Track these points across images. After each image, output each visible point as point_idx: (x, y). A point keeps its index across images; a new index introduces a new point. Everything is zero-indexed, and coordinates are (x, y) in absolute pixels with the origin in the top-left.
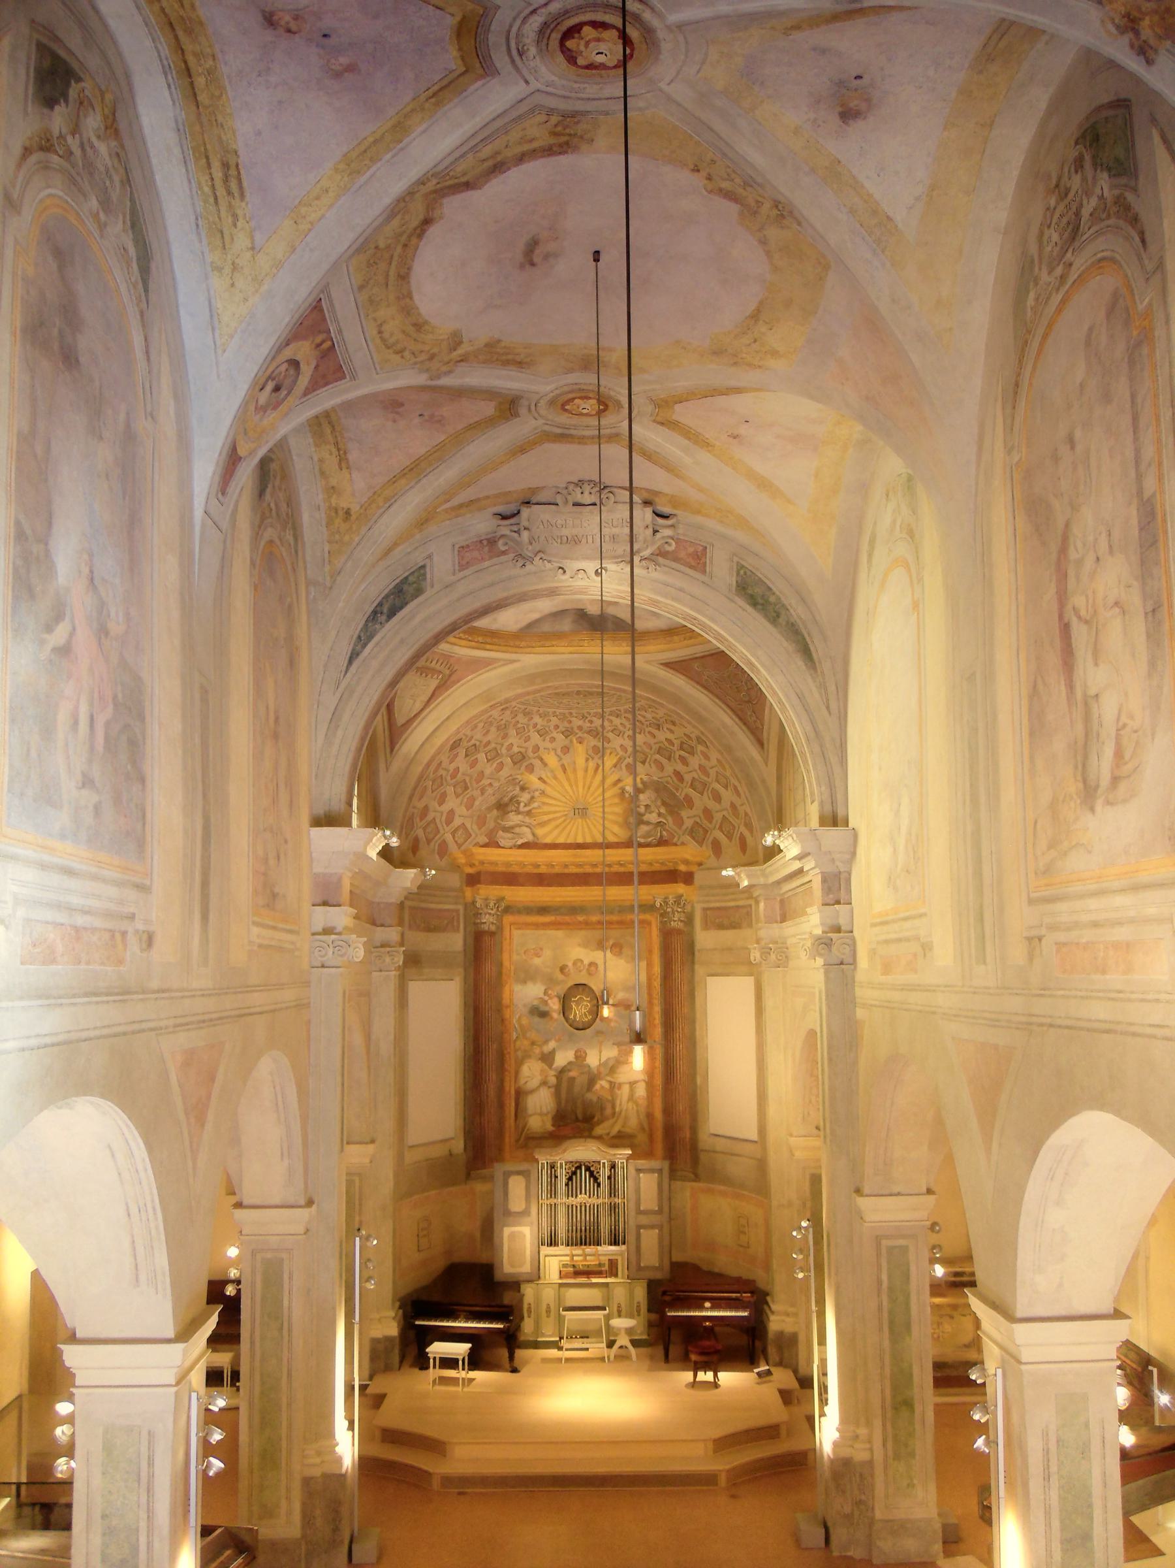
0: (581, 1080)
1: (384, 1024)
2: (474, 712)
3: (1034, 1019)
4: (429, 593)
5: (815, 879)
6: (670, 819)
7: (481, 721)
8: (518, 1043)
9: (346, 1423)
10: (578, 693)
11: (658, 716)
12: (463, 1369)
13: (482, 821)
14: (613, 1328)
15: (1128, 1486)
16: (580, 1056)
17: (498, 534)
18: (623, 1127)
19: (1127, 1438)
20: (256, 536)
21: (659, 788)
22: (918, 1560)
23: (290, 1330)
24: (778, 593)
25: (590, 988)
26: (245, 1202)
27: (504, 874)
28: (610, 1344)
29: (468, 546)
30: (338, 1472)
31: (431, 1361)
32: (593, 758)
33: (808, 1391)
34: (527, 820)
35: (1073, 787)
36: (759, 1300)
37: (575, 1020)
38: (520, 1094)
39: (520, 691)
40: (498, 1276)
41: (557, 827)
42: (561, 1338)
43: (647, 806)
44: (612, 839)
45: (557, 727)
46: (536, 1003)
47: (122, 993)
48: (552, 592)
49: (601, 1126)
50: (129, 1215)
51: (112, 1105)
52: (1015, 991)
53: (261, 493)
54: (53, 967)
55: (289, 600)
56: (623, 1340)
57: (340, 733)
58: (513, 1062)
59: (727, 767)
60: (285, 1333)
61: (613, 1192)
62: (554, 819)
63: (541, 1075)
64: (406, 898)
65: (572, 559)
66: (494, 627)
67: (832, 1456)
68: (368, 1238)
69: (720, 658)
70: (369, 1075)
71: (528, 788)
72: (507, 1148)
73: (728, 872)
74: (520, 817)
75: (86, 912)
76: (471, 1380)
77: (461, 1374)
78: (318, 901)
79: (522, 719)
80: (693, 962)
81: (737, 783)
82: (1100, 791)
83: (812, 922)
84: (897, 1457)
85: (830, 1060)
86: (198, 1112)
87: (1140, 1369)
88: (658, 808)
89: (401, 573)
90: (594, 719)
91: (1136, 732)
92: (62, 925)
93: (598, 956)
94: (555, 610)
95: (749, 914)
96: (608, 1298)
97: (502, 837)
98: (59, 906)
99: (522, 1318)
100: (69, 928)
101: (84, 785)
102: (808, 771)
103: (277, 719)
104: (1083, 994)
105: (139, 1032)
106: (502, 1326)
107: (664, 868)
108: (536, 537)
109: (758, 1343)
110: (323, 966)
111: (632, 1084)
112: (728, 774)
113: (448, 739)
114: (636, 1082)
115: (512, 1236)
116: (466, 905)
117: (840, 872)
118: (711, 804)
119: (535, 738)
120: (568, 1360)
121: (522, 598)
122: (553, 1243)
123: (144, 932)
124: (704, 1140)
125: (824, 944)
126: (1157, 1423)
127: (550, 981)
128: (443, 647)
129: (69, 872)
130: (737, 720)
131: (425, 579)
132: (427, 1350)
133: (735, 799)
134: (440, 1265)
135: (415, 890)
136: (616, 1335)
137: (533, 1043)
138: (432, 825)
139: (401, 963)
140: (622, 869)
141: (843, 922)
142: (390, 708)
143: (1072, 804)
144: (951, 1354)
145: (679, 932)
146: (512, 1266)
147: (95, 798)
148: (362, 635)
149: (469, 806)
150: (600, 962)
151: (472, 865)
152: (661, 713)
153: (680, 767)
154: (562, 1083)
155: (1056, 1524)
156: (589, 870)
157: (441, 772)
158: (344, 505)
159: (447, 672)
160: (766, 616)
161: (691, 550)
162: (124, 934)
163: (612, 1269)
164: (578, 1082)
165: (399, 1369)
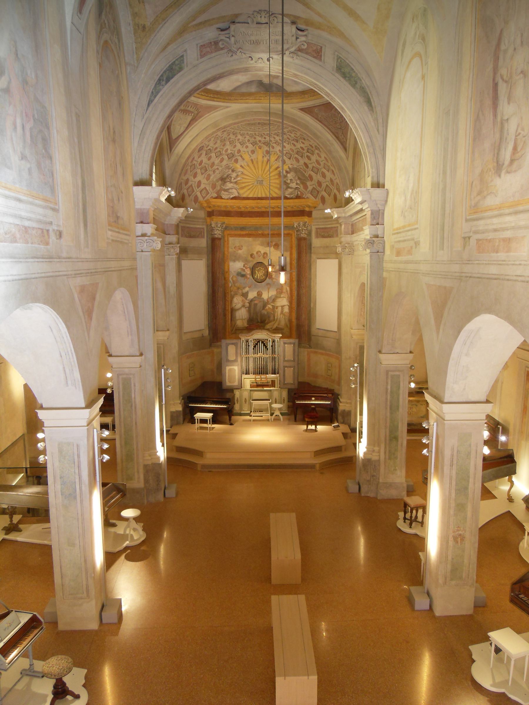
0: (260, 305)
1: (171, 278)
2: (210, 132)
3: (463, 274)
4: (186, 69)
5: (368, 213)
6: (302, 186)
7: (212, 137)
8: (231, 288)
9: (161, 444)
10: (259, 123)
11: (297, 136)
12: (210, 424)
13: (214, 186)
14: (273, 408)
15: (485, 472)
16: (260, 294)
17: (219, 39)
18: (278, 325)
19: (486, 451)
20: (99, 37)
21: (296, 171)
22: (396, 498)
23: (135, 408)
24: (356, 71)
26: (113, 354)
27: (225, 211)
28: (272, 414)
29: (204, 45)
30: (157, 462)
31: (196, 420)
32: (266, 156)
33: (354, 433)
34: (235, 186)
36: (335, 397)
37: (257, 278)
38: (233, 311)
39: (231, 122)
40: (224, 387)
41: (249, 189)
42: (251, 412)
43: (291, 180)
46: (239, 270)
47: (49, 258)
48: (246, 70)
49: (269, 325)
50: (61, 356)
51: (49, 308)
52: (456, 262)
53: (100, 15)
54: (15, 244)
55: (117, 72)
56: (277, 413)
57: (145, 141)
58: (230, 296)
59: (329, 161)
61: (273, 352)
62: (248, 185)
63: (242, 302)
64: (180, 222)
65: (255, 52)
66: (218, 89)
67: (363, 458)
68: (167, 369)
69: (328, 106)
70: (166, 302)
71: (235, 171)
72: (227, 334)
73: (328, 211)
74: (232, 184)
75: (29, 219)
76: (213, 428)
77: (209, 426)
78: (138, 221)
79: (232, 137)
80: (311, 253)
81: (333, 169)
83: (366, 233)
84: (390, 458)
85: (370, 294)
86: (89, 313)
87: (494, 427)
88: (296, 181)
90: (266, 137)
92: (18, 225)
93: (267, 250)
94: (247, 81)
95: (337, 231)
96: (271, 396)
97: (223, 194)
98: (15, 216)
99: (235, 404)
100: (21, 226)
101: (22, 159)
102: (367, 162)
103: (114, 132)
104: (487, 262)
105: (59, 276)
106: (226, 407)
108: (238, 41)
109: (334, 414)
110: (142, 251)
111: (282, 307)
112: (329, 164)
113: (197, 146)
114: (284, 306)
115: (230, 370)
116: (207, 226)
117: (379, 210)
118: (321, 179)
119: (239, 146)
120: (254, 420)
121: (231, 73)
122: (248, 373)
123: (57, 230)
124: (314, 331)
125: (370, 243)
126: (499, 448)
127: (246, 261)
128: (192, 99)
129: (19, 200)
130: (335, 138)
131: (183, 62)
132: (194, 416)
133: (332, 176)
134: (199, 382)
135: (184, 218)
136: (274, 411)
138: (191, 188)
139: (178, 252)
141: (380, 233)
142: (169, 128)
143: (490, 173)
144: (415, 420)
145: (305, 239)
146: (230, 382)
147: (28, 166)
148: (154, 91)
149: (208, 179)
150: (268, 252)
151: (210, 207)
152: (298, 134)
153: (307, 161)
154: (252, 306)
155: (454, 483)
156: (264, 210)
157: (194, 162)
160: (350, 84)
161: (315, 48)
163: (273, 384)
165: (183, 423)
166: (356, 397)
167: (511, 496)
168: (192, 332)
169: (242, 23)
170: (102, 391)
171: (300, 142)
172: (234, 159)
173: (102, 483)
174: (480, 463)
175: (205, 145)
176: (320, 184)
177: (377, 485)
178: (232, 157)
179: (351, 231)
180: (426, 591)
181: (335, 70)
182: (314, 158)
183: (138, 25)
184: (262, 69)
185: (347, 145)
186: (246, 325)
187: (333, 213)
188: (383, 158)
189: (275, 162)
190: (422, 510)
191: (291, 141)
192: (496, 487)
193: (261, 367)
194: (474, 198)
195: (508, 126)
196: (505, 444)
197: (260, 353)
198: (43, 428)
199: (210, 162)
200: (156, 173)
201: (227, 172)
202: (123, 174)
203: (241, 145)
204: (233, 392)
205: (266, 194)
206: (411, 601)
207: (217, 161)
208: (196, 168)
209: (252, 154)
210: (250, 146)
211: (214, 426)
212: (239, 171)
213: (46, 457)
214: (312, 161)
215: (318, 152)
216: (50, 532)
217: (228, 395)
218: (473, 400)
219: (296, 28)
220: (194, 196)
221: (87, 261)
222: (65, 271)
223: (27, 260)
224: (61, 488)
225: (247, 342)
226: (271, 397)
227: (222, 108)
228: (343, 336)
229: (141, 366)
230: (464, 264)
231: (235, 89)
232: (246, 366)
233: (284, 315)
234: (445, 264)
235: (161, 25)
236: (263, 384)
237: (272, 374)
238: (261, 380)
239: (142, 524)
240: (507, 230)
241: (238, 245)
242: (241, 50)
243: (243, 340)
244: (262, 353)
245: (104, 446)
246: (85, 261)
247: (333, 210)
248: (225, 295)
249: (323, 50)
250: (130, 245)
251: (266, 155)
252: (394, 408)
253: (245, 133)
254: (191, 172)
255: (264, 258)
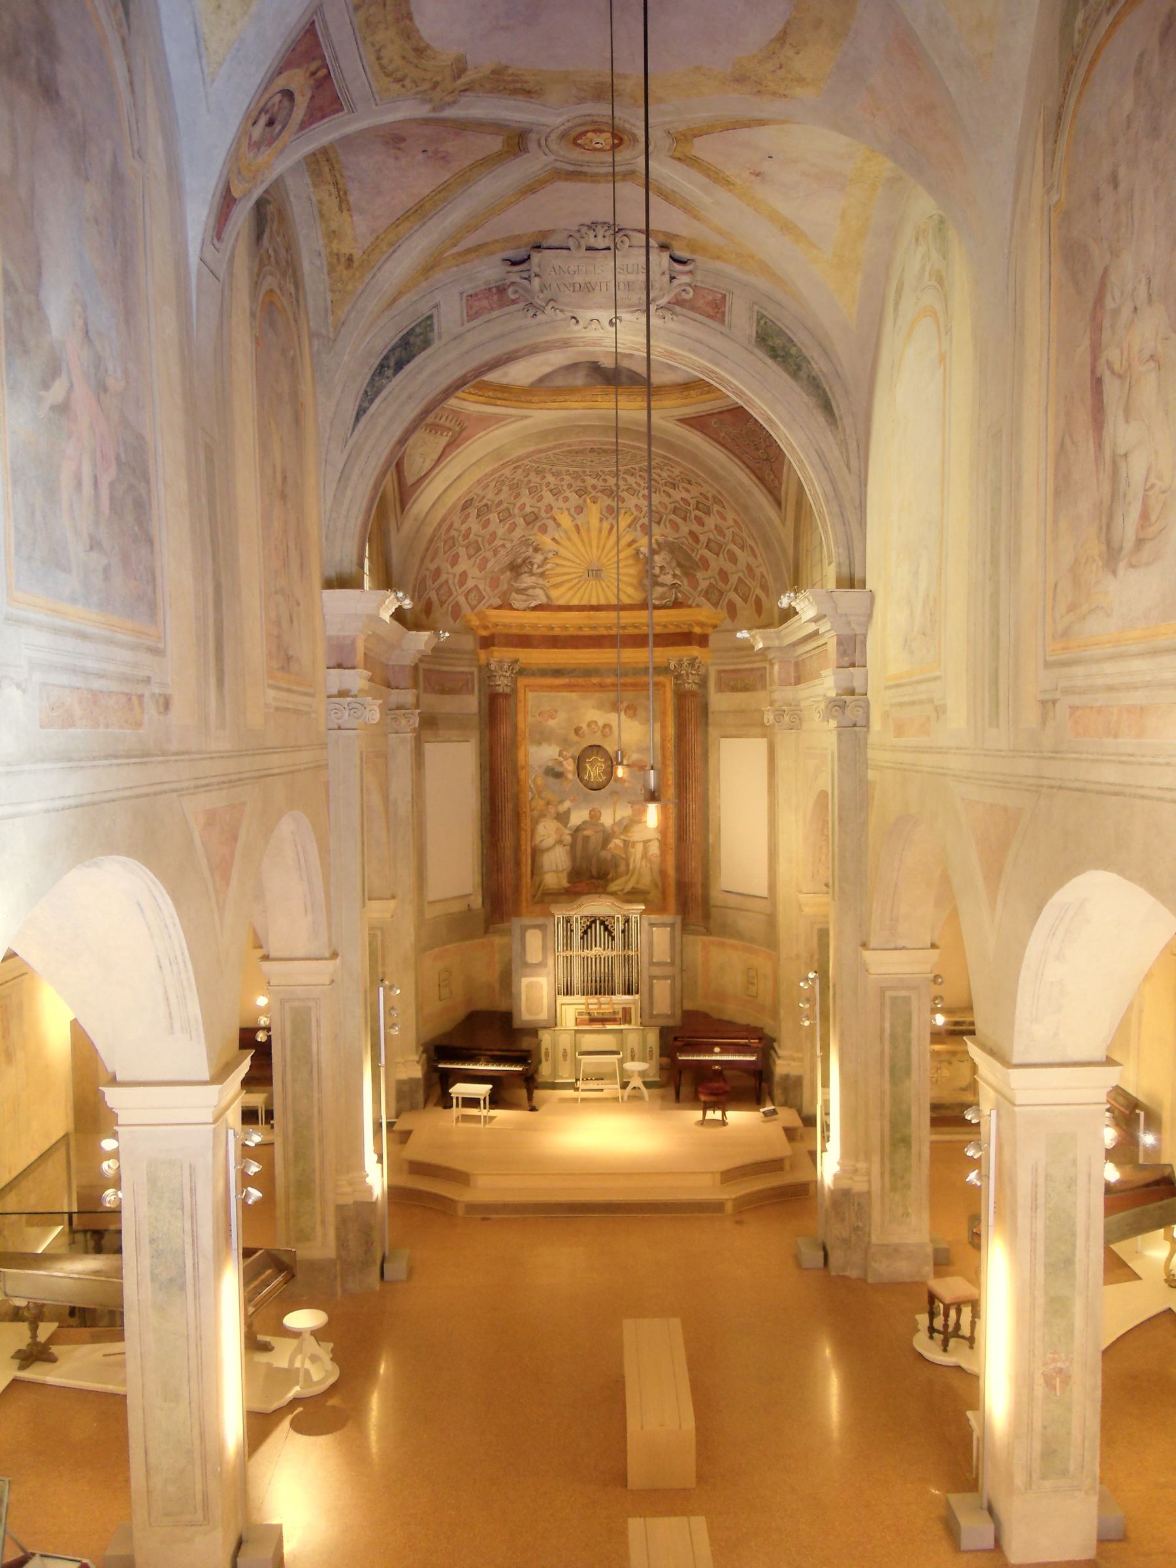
0: (595, 839)
1: (401, 784)
3: (1045, 782)
4: (436, 344)
6: (685, 581)
7: (491, 481)
8: (534, 804)
9: (375, 1157)
10: (592, 450)
11: (674, 475)
12: (485, 1108)
13: (494, 583)
14: (627, 1071)
16: (595, 816)
19: (1112, 1173)
20: (255, 285)
21: (673, 549)
24: (799, 344)
25: (606, 752)
26: (273, 954)
28: (624, 1086)
29: (476, 294)
31: (454, 1100)
32: (607, 518)
33: (811, 1129)
34: (541, 581)
35: (1095, 549)
36: (766, 1045)
38: (536, 852)
39: (531, 449)
40: (517, 1024)
42: (577, 1080)
43: (662, 568)
44: (626, 600)
45: (570, 486)
46: (550, 764)
47: (143, 755)
48: (565, 344)
50: (161, 967)
52: (1026, 754)
53: (259, 238)
55: (292, 353)
56: (636, 1082)
57: (349, 492)
60: (315, 1075)
61: (626, 945)
62: (570, 580)
64: (421, 660)
68: (391, 987)
69: (738, 414)
73: (743, 634)
74: (534, 579)
75: (101, 676)
76: (492, 1118)
77: (482, 1112)
78: (332, 663)
79: (533, 476)
80: (706, 724)
81: (752, 543)
82: (1124, 552)
83: (827, 684)
84: (894, 1189)
85: (841, 819)
87: (1127, 1112)
89: (407, 323)
90: (608, 477)
91: (1163, 492)
92: (78, 688)
93: (612, 718)
95: (763, 677)
96: (622, 1043)
97: (515, 600)
99: (540, 1062)
100: (85, 692)
101: (91, 548)
102: (826, 532)
103: (285, 478)
105: (161, 793)
106: (521, 1069)
107: (679, 630)
108: (547, 285)
109: (764, 1085)
110: (339, 728)
111: (646, 843)
112: (744, 535)
115: (530, 986)
116: (480, 667)
117: (856, 635)
118: (728, 566)
119: (548, 498)
120: (584, 1100)
121: (533, 350)
122: (569, 992)
123: (160, 695)
124: (716, 896)
125: (837, 706)
126: (1141, 1161)
127: (565, 742)
128: (453, 402)
129: (82, 636)
130: (755, 479)
132: (450, 1091)
133: (751, 560)
134: (460, 1014)
135: (430, 653)
136: (630, 1077)
137: (548, 803)
138: (445, 587)
140: (636, 631)
141: (857, 684)
142: (399, 466)
144: (947, 1097)
145: (693, 694)
148: (369, 389)
149: (482, 567)
150: (614, 724)
151: (486, 628)
152: (677, 471)
153: (696, 528)
154: (578, 840)
156: (603, 632)
157: (453, 533)
158: (345, 250)
159: (458, 429)
161: (710, 298)
162: (141, 697)
163: (626, 1017)
164: (593, 839)
166: (813, 1046)
167: (1172, 1273)
168: (446, 900)
169: (556, 248)
170: (247, 1038)
171: (681, 488)
172: (539, 524)
173: (243, 1249)
174: (1098, 1200)
175: (476, 497)
176: (723, 575)
177: (866, 1251)
178: (534, 520)
179: (795, 677)
180: (985, 1505)
181: (754, 341)
182: (711, 521)
183: (338, 255)
184: (597, 341)
185: (783, 494)
186: (565, 883)
187: (755, 639)
188: (861, 524)
189: (628, 530)
190: (970, 1308)
191: (660, 486)
192: (1138, 1253)
193: (598, 979)
194: (1062, 617)
195: (1127, 467)
196: (1156, 1151)
197: (596, 946)
198: (115, 1128)
199: (486, 533)
200: (370, 558)
201: (524, 552)
202: (302, 565)
203: (554, 495)
204: (537, 1036)
205: (607, 598)
206: (951, 1528)
207: (501, 531)
208: (457, 546)
209: (578, 514)
210: (573, 497)
211: (493, 1113)
212: (550, 551)
213: (119, 1192)
214: (706, 529)
215: (721, 510)
216: (123, 1365)
217: (526, 1043)
218: (1077, 1057)
219: (671, 257)
220: (452, 604)
221: (222, 757)
222: (175, 782)
223: (95, 763)
224: (152, 1265)
225: (568, 922)
226: (622, 1046)
227: (512, 419)
228: (781, 908)
229: (333, 981)
230: (1045, 758)
231: (541, 380)
232: (565, 976)
233: (649, 861)
234: (1004, 757)
235: (386, 255)
236: (605, 1017)
237: (625, 994)
238: (600, 1008)
239: (331, 1345)
240: (1136, 688)
241: (548, 709)
242: (555, 304)
243: (558, 918)
244: (600, 946)
245: (249, 1167)
246: (218, 757)
247: (754, 632)
248: (518, 816)
249: (727, 303)
250: (313, 715)
251: (608, 515)
252: (899, 1071)
253: (561, 471)
254: (445, 553)
255: (604, 736)
